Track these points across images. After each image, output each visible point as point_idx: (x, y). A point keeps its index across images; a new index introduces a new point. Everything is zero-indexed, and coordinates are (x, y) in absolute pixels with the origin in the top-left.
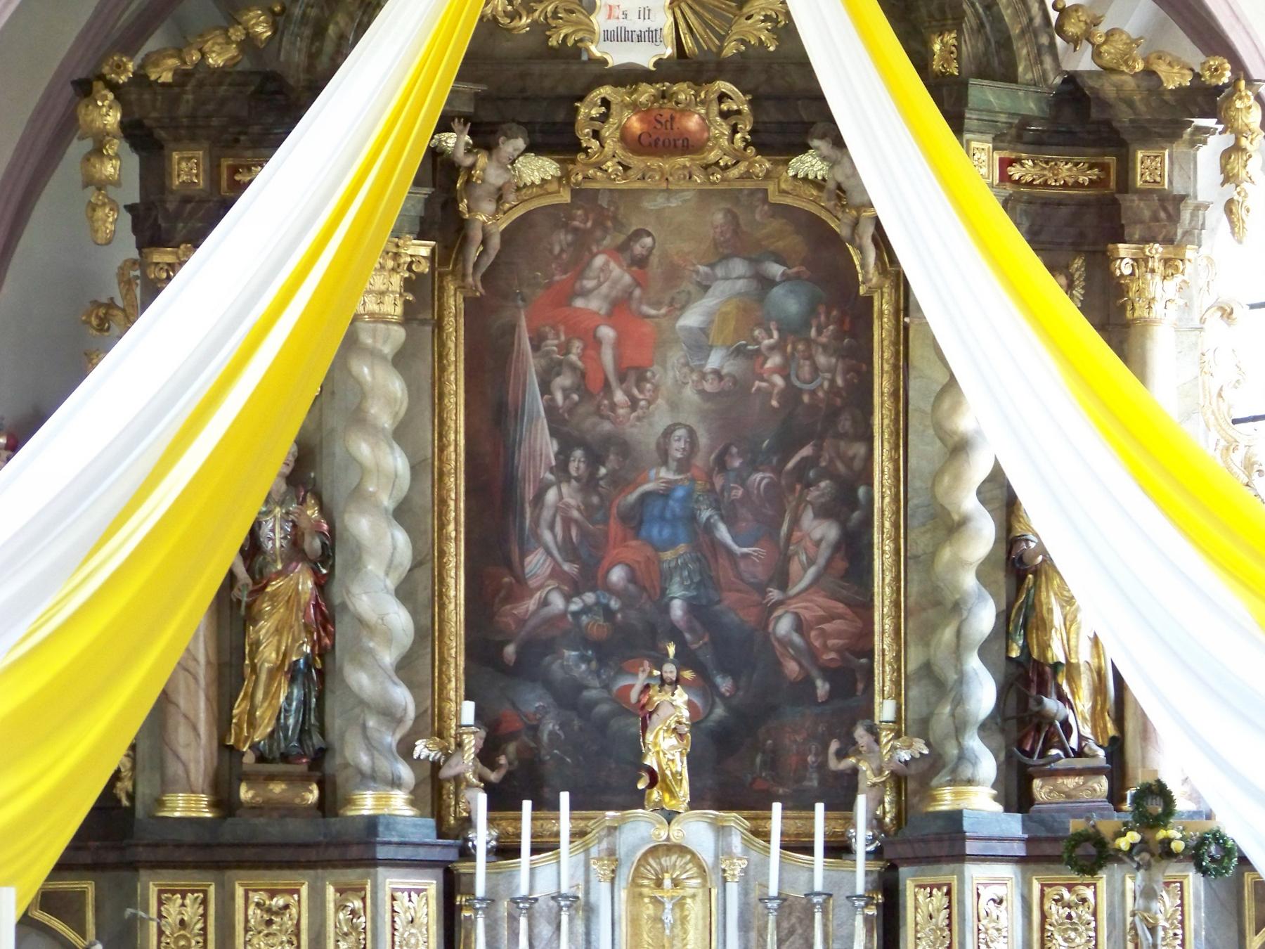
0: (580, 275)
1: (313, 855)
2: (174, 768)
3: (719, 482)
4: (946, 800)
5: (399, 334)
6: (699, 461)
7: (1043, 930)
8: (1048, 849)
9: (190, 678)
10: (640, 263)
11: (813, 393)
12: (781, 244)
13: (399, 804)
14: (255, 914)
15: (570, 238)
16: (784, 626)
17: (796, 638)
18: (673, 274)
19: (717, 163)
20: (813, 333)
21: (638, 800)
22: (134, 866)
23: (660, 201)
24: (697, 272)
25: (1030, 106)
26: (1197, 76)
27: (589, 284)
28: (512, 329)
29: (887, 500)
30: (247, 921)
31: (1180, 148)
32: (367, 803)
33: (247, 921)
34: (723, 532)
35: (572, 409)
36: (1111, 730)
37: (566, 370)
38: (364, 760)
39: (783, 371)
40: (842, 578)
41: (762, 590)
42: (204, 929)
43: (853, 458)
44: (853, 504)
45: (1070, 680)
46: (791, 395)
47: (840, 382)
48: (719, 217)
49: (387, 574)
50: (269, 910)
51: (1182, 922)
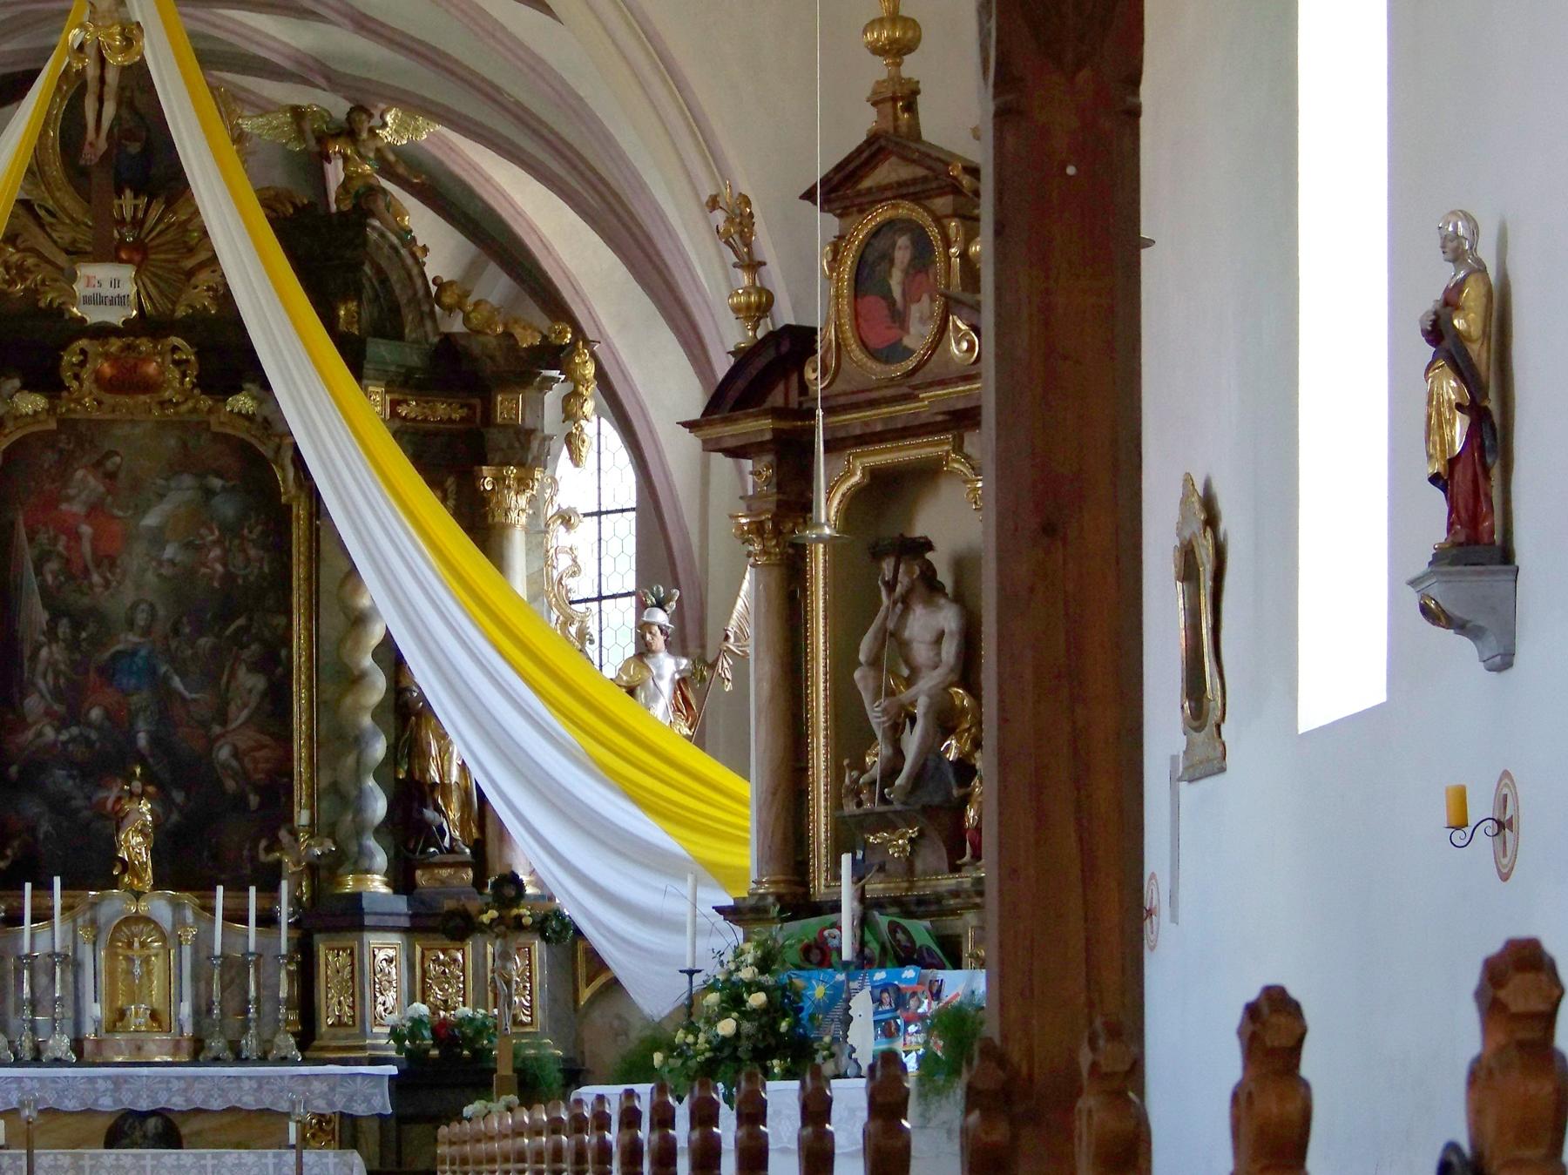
3: (173, 644)
4: (350, 885)
11: (245, 578)
16: (224, 753)
17: (234, 763)
18: (136, 486)
25: (414, 360)
27: (72, 492)
28: (12, 524)
29: (303, 659)
31: (531, 393)
34: (177, 682)
35: (59, 588)
36: (475, 833)
41: (205, 725)
46: (229, 577)
47: (266, 569)
48: (173, 442)
51: (530, 977)
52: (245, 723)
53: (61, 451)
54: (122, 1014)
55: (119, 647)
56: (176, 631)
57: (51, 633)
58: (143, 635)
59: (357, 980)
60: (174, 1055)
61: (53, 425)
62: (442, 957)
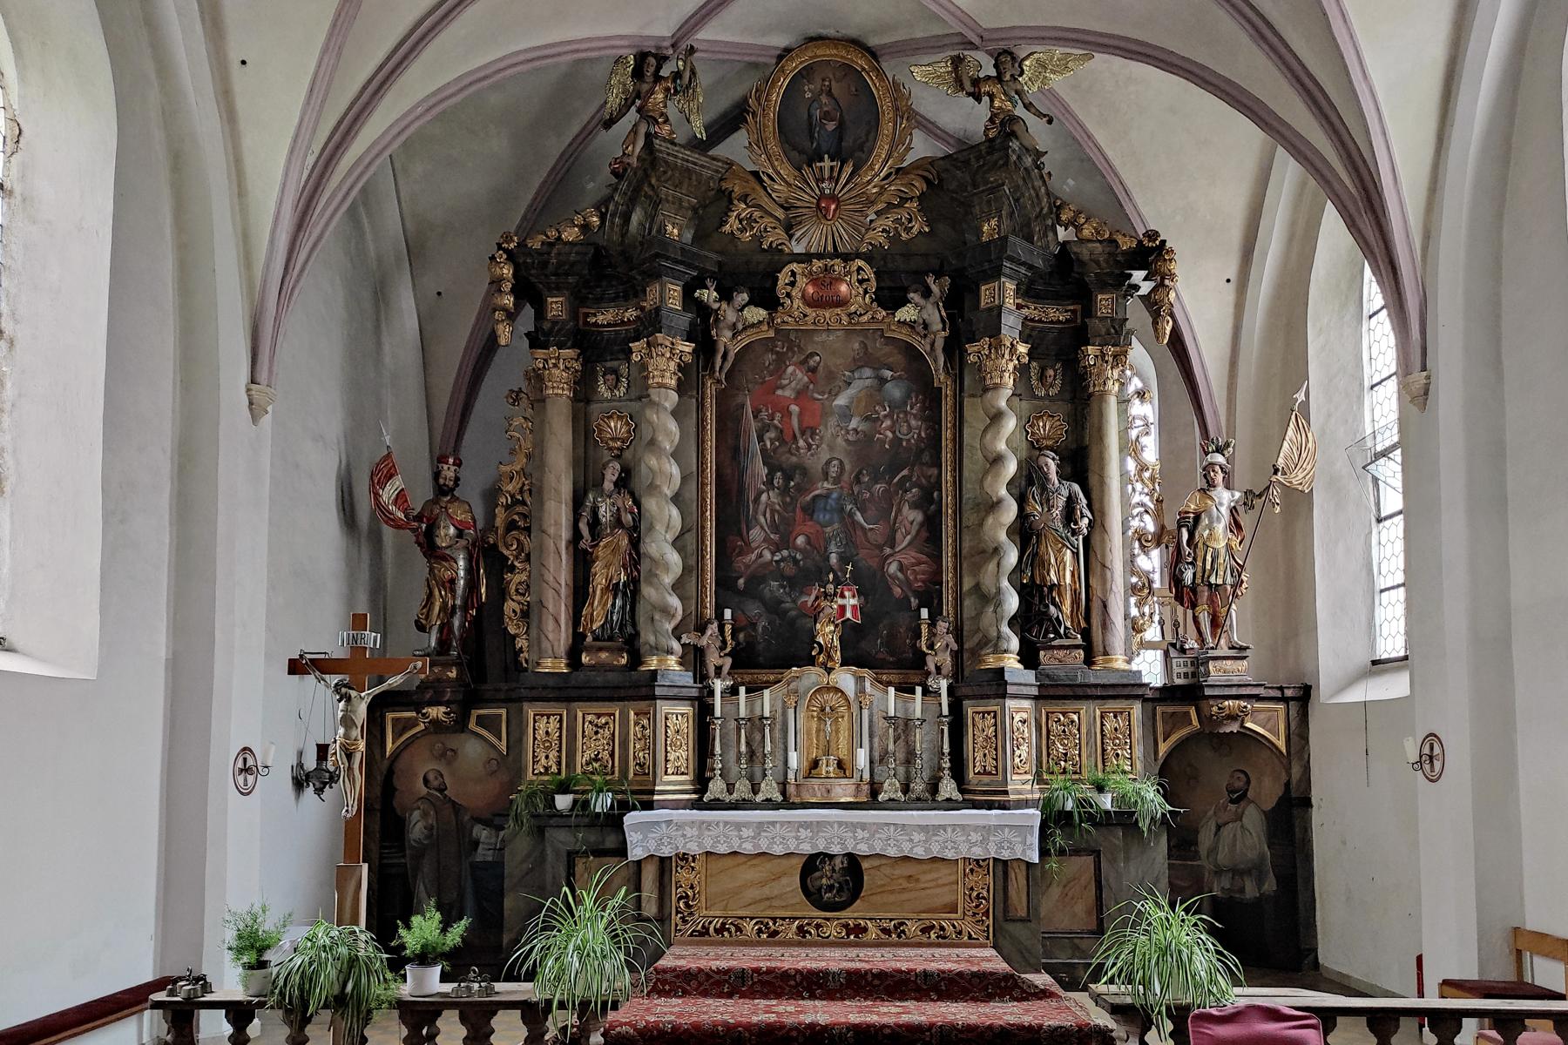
0: (780, 378)
1: (623, 693)
2: (546, 645)
3: (856, 489)
4: (991, 662)
5: (674, 396)
6: (845, 477)
7: (1048, 738)
8: (1052, 692)
9: (556, 595)
10: (813, 370)
11: (909, 440)
12: (891, 360)
13: (672, 662)
14: (589, 729)
15: (774, 357)
16: (893, 568)
17: (900, 575)
18: (831, 376)
19: (855, 313)
20: (909, 408)
21: (812, 661)
22: (520, 700)
23: (824, 336)
24: (844, 375)
26: (1140, 242)
27: (785, 382)
28: (743, 406)
29: (950, 498)
30: (584, 732)
32: (653, 663)
33: (584, 732)
34: (859, 517)
35: (775, 450)
36: (1083, 624)
37: (772, 429)
38: (652, 639)
39: (892, 429)
40: (925, 541)
41: (880, 548)
42: (560, 736)
43: (930, 476)
44: (931, 501)
45: (1060, 594)
46: (896, 441)
47: (923, 435)
48: (856, 346)
49: (666, 532)
50: (596, 726)
51: (1130, 735)
52: (909, 544)
53: (777, 353)
54: (815, 764)
55: (817, 492)
56: (858, 480)
57: (769, 483)
58: (834, 484)
59: (999, 737)
60: (856, 796)
61: (771, 334)
62: (1062, 718)
